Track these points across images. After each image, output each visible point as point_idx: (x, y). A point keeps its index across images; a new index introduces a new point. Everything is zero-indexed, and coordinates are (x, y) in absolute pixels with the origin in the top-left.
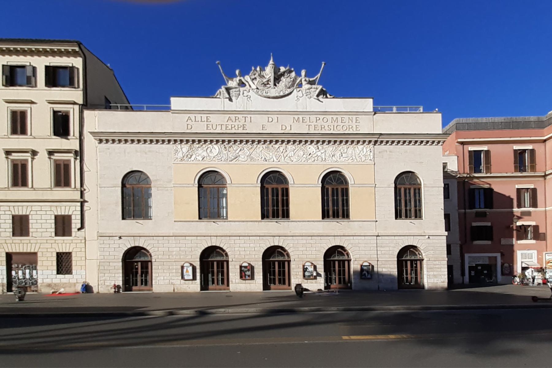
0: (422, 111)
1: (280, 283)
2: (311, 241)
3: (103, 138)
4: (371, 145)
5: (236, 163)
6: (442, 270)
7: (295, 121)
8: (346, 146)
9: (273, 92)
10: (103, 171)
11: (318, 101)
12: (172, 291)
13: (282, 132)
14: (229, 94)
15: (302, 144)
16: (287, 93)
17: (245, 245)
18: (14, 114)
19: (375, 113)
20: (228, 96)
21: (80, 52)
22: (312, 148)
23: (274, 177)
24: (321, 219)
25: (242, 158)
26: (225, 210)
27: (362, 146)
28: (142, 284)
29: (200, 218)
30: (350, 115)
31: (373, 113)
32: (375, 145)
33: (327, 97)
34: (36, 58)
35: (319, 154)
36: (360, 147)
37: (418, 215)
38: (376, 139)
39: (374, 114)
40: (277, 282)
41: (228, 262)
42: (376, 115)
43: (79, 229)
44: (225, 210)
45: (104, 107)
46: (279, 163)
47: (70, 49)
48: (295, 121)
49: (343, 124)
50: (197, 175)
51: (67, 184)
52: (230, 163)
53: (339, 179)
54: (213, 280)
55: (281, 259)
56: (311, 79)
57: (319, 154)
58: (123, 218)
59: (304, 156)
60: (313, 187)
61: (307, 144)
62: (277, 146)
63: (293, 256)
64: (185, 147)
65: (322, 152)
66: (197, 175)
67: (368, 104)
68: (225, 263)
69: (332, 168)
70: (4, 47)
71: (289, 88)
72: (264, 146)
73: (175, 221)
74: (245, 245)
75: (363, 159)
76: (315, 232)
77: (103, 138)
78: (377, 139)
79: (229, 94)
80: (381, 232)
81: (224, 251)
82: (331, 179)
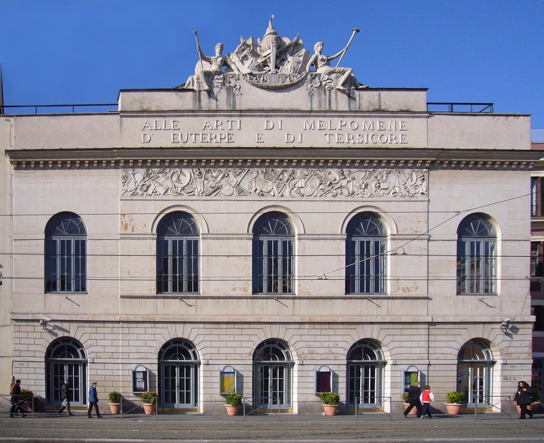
5: (215, 198)
25: (227, 190)
46: (282, 199)
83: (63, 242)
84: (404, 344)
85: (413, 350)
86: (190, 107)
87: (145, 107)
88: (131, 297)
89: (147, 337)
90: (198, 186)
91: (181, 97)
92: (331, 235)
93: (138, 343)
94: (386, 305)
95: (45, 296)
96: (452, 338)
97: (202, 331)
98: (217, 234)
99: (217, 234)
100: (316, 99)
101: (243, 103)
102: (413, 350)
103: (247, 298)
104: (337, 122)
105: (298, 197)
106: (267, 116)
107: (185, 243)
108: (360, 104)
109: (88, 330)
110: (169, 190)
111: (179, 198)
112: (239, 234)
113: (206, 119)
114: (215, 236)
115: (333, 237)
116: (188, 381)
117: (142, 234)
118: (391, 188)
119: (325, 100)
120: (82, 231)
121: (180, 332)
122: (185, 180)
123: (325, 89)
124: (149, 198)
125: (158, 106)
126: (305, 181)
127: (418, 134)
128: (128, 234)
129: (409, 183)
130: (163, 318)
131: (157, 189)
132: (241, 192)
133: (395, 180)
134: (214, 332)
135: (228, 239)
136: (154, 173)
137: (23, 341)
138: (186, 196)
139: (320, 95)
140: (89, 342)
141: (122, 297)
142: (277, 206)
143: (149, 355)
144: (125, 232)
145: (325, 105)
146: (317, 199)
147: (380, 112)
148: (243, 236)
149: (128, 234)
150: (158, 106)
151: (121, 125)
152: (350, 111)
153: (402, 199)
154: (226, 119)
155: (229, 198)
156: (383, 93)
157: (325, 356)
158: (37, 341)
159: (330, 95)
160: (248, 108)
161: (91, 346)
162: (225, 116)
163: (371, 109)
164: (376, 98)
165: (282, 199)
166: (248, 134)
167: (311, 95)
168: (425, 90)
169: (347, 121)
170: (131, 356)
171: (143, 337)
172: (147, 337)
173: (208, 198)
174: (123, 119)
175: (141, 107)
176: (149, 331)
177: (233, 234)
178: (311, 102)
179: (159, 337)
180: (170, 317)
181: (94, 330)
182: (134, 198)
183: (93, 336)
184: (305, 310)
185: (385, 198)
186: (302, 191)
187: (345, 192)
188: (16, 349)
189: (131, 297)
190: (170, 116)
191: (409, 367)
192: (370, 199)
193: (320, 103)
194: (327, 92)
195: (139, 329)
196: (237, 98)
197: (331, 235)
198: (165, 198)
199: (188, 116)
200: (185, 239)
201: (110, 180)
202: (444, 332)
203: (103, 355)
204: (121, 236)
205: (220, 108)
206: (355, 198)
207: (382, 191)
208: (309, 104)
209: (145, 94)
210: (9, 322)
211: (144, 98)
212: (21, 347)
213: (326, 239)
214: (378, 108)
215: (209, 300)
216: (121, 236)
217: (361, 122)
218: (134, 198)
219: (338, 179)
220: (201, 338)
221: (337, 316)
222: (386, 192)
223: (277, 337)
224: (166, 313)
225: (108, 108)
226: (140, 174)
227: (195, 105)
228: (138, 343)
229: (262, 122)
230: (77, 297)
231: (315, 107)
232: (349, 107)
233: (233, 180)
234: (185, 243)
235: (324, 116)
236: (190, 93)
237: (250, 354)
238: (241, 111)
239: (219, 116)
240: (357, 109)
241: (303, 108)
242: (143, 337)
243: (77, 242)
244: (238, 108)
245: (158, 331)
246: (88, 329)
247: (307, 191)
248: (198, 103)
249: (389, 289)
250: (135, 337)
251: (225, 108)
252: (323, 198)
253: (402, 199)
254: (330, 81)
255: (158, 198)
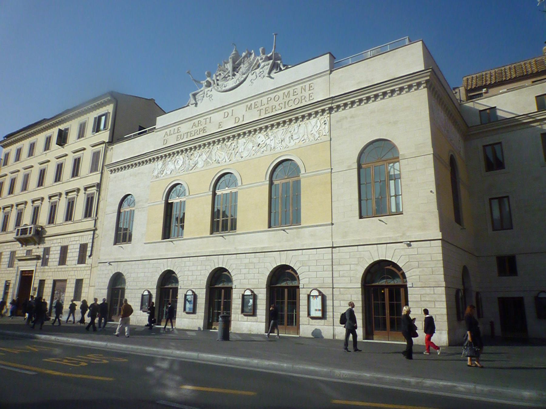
0: (407, 43)
2: (255, 260)
4: (326, 115)
5: (195, 171)
6: (437, 305)
7: (248, 109)
8: (296, 124)
9: (231, 83)
11: (269, 78)
12: (332, 338)
14: (195, 99)
15: (251, 135)
16: (242, 79)
17: (194, 268)
19: (331, 72)
20: (194, 102)
22: (260, 138)
24: (209, 235)
26: (393, 199)
27: (316, 119)
29: (270, 227)
30: (302, 83)
31: (329, 72)
32: (330, 113)
33: (281, 70)
36: (313, 121)
38: (330, 105)
39: (330, 73)
41: (405, 287)
42: (333, 72)
44: (393, 199)
46: (230, 162)
48: (285, 97)
49: (295, 97)
51: (90, 216)
52: (191, 172)
56: (269, 55)
58: (361, 217)
59: (254, 148)
60: (257, 186)
61: (257, 133)
62: (229, 143)
63: (236, 284)
64: (160, 163)
65: (272, 139)
67: (323, 62)
68: (402, 290)
69: (172, 182)
71: (244, 74)
72: (219, 146)
73: (145, 243)
74: (194, 268)
75: (317, 136)
76: (259, 246)
78: (331, 105)
79: (195, 99)
80: (338, 242)
81: (399, 269)
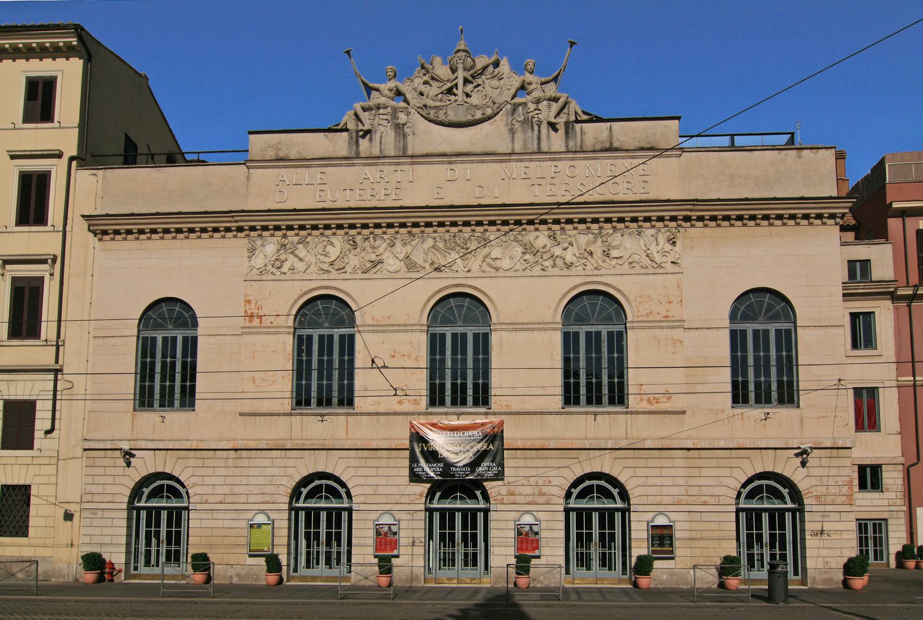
1: (328, 562)
3: (104, 227)
5: (376, 276)
10: (103, 295)
13: (320, 206)
18: (26, 179)
21: (81, 48)
23: (171, 311)
25: (392, 263)
28: (466, 564)
34: (61, 61)
35: (558, 251)
37: (788, 395)
40: (595, 563)
41: (350, 511)
43: (48, 432)
45: (121, 159)
46: (469, 275)
47: (61, 42)
50: (295, 302)
53: (180, 316)
54: (148, 554)
55: (335, 504)
57: (558, 251)
66: (295, 302)
70: (6, 43)
77: (104, 227)
82: (317, 314)
83: (165, 339)
84: (651, 481)
85: (665, 490)
86: (344, 152)
87: (282, 154)
88: (254, 415)
89: (274, 471)
90: (353, 261)
91: (331, 140)
92: (539, 323)
93: (261, 480)
94: (624, 423)
95: (134, 416)
96: (727, 472)
97: (352, 462)
98: (376, 326)
99: (376, 326)
100: (519, 137)
101: (415, 146)
102: (665, 490)
103: (284, 414)
104: (548, 167)
105: (492, 272)
106: (450, 163)
107: (316, 339)
108: (582, 142)
109: (192, 462)
110: (313, 267)
111: (325, 276)
112: (408, 325)
113: (367, 170)
114: (375, 328)
115: (542, 326)
116: (783, 536)
117: (519, 324)
118: (625, 258)
119: (532, 138)
120: (351, 321)
121: (322, 463)
122: (334, 252)
123: (532, 123)
124: (283, 277)
125: (299, 153)
126: (505, 251)
127: (666, 180)
128: (253, 327)
129: (653, 249)
130: (297, 444)
131: (295, 265)
132: (411, 265)
133: (629, 244)
134: (370, 463)
135: (393, 331)
136: (292, 244)
137: (98, 480)
138: (334, 274)
139: (525, 132)
140: (193, 480)
141: (241, 414)
142: (463, 285)
143: (117, 499)
144: (250, 325)
145: (532, 144)
146: (520, 273)
147: (281, 161)
148: (414, 328)
149: (253, 327)
150: (299, 153)
151: (248, 178)
152: (568, 152)
153: (643, 271)
154: (394, 168)
155: (394, 275)
156: (616, 126)
157: (531, 499)
158: (118, 480)
159: (539, 132)
160: (424, 152)
161: (194, 485)
162: (391, 164)
163: (598, 147)
164: (605, 134)
165: (469, 275)
166: (421, 187)
167: (512, 132)
168: (678, 118)
169: (563, 166)
170: (252, 499)
171: (269, 471)
172: (274, 471)
173: (366, 276)
174: (252, 171)
175: (277, 154)
176: (278, 462)
177: (399, 325)
178: (513, 141)
179: (291, 471)
180: (307, 442)
181: (200, 462)
182: (264, 277)
183: (199, 471)
184: (648, 431)
185: (619, 270)
186: (498, 263)
187: (559, 262)
188: (87, 491)
189: (254, 415)
190: (315, 166)
191: (381, 514)
192: (596, 272)
193: (524, 141)
194: (536, 128)
195: (263, 459)
196: (410, 139)
197: (539, 323)
198: (306, 277)
199: (341, 165)
200: (337, 332)
201: (228, 253)
202: (714, 463)
203: (211, 499)
204: (244, 330)
205: (387, 153)
206: (573, 271)
207: (615, 261)
208: (510, 144)
209: (283, 136)
210: (79, 452)
211: (280, 142)
212: (94, 489)
213: (533, 330)
214: (608, 146)
215: (640, 416)
216: (244, 330)
217: (582, 166)
218: (264, 277)
219: (549, 245)
220: (352, 472)
221: (547, 439)
222: (620, 261)
223: (599, 470)
224: (304, 437)
225: (239, 156)
226: (272, 245)
227: (350, 149)
228: (261, 480)
229: (440, 171)
230: (782, 413)
231: (518, 148)
232: (567, 146)
233: (401, 250)
234: (316, 339)
235: (531, 160)
236: (345, 134)
237: (421, 495)
238: (412, 156)
239: (383, 164)
240: (578, 149)
241: (501, 150)
242: (269, 471)
243: (185, 339)
244: (409, 152)
245: (291, 462)
246: (192, 460)
247: (506, 263)
248: (354, 147)
249: (632, 401)
250: (257, 471)
251: (392, 153)
252: (528, 273)
253: (643, 271)
254: (537, 112)
255: (296, 277)
